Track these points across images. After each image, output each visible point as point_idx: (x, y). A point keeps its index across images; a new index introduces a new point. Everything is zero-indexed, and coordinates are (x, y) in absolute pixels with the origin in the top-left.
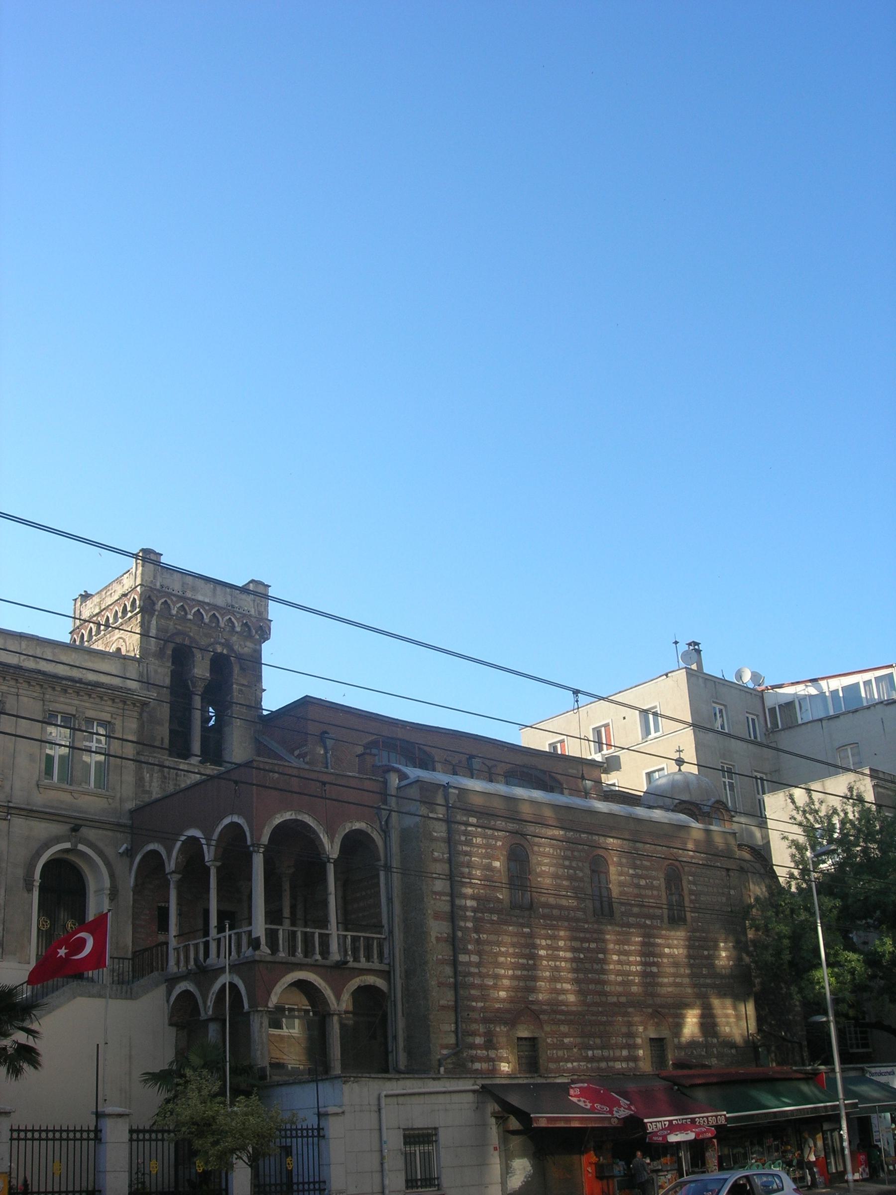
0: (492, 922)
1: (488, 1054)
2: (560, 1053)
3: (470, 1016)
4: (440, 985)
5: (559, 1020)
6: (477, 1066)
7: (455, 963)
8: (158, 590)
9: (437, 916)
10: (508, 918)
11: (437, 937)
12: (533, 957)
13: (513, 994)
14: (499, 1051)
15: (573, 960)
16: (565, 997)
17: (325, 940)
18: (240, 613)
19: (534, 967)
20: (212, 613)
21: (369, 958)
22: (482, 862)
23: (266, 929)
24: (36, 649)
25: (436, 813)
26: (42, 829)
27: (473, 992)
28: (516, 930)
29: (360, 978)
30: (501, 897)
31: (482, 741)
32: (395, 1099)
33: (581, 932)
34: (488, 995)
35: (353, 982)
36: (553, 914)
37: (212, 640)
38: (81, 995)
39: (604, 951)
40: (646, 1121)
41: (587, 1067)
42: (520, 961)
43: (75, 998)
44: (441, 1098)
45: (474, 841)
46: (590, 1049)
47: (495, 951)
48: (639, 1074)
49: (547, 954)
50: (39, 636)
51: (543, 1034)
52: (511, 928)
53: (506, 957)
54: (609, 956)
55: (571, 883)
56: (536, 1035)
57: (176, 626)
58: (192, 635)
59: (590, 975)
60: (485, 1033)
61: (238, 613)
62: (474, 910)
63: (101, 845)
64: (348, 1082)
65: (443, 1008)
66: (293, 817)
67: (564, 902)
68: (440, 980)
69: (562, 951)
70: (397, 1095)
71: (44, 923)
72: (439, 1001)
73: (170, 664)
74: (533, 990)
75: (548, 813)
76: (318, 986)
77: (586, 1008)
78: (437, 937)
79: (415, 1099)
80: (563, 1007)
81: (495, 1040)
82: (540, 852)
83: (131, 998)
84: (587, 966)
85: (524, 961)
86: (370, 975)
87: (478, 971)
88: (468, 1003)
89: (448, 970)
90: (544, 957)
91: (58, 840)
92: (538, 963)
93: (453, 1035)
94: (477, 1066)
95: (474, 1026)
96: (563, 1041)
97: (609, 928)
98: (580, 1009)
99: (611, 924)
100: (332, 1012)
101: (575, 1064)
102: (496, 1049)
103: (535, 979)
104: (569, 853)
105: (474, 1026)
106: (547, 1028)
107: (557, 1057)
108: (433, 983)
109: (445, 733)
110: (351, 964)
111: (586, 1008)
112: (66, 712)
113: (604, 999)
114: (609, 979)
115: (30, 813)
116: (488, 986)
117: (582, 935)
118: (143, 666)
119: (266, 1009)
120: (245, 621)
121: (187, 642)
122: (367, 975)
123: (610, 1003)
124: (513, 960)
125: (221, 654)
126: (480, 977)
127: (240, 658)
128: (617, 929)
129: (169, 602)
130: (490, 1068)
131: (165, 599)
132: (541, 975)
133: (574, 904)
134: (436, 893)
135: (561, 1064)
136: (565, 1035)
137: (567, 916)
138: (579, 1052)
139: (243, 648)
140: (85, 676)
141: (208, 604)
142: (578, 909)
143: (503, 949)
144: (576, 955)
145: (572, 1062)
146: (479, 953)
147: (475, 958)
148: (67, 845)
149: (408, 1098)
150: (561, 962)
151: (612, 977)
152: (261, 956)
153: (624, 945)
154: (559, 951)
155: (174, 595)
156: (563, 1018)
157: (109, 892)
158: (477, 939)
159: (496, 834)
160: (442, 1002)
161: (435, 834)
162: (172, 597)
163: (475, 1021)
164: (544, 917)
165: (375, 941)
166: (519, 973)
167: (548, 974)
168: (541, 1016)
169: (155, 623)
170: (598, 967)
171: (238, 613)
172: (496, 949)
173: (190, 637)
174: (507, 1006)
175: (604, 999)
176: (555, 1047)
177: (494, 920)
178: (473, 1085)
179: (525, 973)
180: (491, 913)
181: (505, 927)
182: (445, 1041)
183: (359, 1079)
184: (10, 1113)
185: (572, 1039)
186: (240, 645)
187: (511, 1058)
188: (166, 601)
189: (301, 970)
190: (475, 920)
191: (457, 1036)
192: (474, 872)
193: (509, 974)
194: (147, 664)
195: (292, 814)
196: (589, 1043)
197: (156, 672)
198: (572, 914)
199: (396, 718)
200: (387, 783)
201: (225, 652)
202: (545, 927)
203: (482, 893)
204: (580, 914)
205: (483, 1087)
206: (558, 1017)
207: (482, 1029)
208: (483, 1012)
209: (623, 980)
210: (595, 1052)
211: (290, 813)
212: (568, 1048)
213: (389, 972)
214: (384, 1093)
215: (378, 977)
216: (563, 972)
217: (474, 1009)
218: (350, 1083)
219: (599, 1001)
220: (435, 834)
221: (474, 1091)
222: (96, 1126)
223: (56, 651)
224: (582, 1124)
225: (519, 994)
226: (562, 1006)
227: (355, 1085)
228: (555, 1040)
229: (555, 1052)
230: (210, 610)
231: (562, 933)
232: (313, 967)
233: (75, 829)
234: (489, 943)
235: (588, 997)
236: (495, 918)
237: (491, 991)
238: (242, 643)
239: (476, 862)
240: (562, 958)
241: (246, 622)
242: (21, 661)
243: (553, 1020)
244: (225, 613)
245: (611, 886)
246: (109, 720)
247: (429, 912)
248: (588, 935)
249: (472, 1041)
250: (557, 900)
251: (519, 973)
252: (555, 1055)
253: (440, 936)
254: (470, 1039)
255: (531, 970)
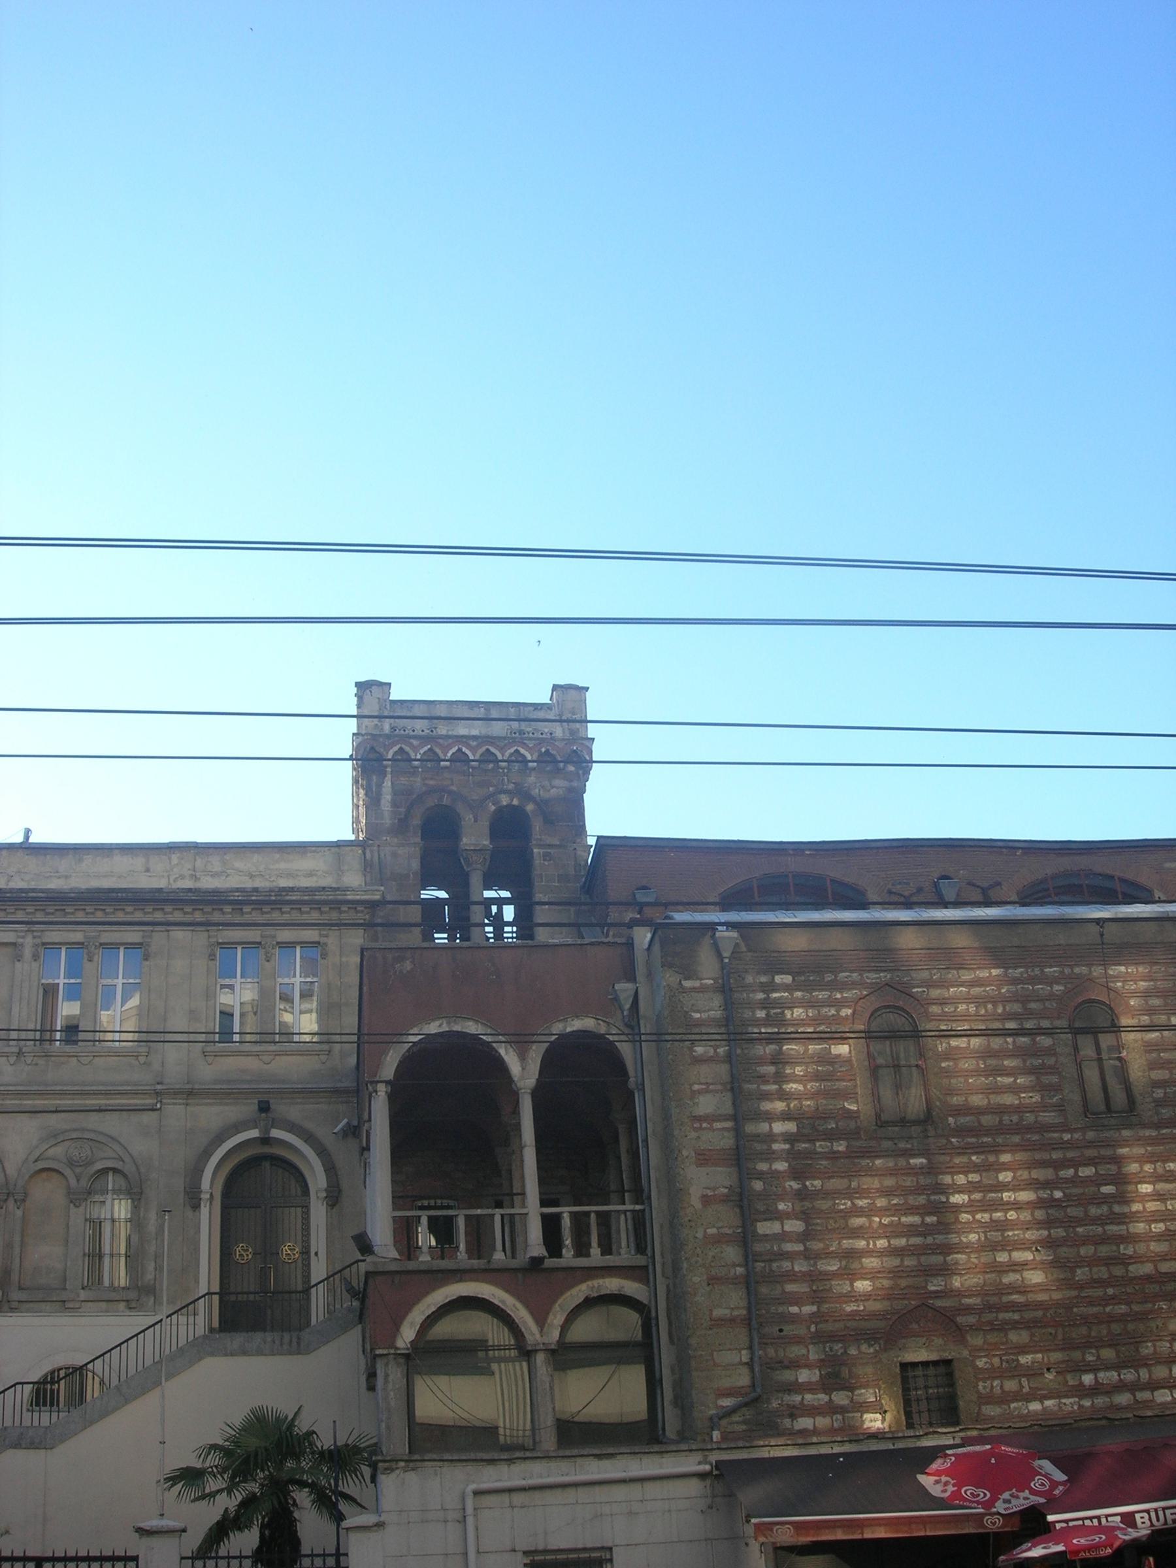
0: (834, 1156)
1: (830, 1399)
2: (1011, 1385)
3: (785, 1333)
4: (713, 1281)
5: (1006, 1322)
6: (805, 1423)
7: (745, 1238)
8: (387, 737)
9: (704, 1159)
10: (873, 1143)
11: (704, 1197)
12: (942, 1210)
13: (886, 1283)
14: (857, 1392)
15: (1039, 1204)
16: (1018, 1276)
17: (513, 1225)
18: (535, 739)
19: (944, 1227)
20: (484, 749)
21: (607, 1249)
22: (807, 1050)
23: (395, 1219)
24: (195, 860)
25: (698, 979)
26: (212, 1115)
27: (790, 1288)
28: (891, 1164)
29: (590, 1283)
30: (854, 1107)
31: (964, 846)
32: (505, 1498)
33: (1054, 1149)
34: (830, 1290)
35: (574, 1291)
36: (982, 1126)
37: (491, 789)
38: (212, 1354)
39: (1120, 1180)
40: (1050, 1518)
41: (1081, 1407)
42: (903, 1219)
43: (200, 1359)
44: (619, 1492)
45: (789, 1016)
46: (1086, 1372)
47: (842, 1207)
48: (1149, 1413)
49: (970, 1200)
50: (198, 841)
51: (966, 1353)
52: (878, 1162)
53: (868, 1216)
54: (1131, 1188)
55: (1024, 1061)
56: (947, 1355)
57: (427, 782)
58: (454, 788)
59: (1080, 1230)
60: (822, 1360)
61: (530, 739)
62: (789, 1138)
63: (310, 1125)
64: (392, 1470)
65: (719, 1322)
66: (445, 1028)
67: (1009, 1099)
68: (713, 1273)
69: (1008, 1191)
70: (510, 1490)
71: (242, 1252)
72: (711, 1310)
73: (418, 840)
74: (946, 1271)
75: (960, 940)
76: (500, 1304)
77: (1074, 1293)
78: (704, 1197)
79: (550, 1497)
80: (1014, 1297)
81: (845, 1372)
82: (944, 1014)
83: (299, 1349)
84: (1072, 1212)
85: (916, 1219)
86: (611, 1276)
87: (802, 1248)
88: (780, 1309)
89: (732, 1253)
90: (963, 1205)
91: (237, 1128)
92: (950, 1218)
93: (745, 1371)
94: (805, 1423)
95: (796, 1351)
96: (1018, 1360)
97: (1126, 1133)
98: (1057, 1296)
99: (1129, 1126)
100: (529, 1348)
101: (1048, 1403)
102: (851, 1389)
103: (947, 1249)
104: (1016, 1007)
105: (796, 1351)
106: (977, 1341)
107: (1003, 1391)
108: (696, 1279)
109: (886, 848)
110: (550, 1263)
111: (1074, 1293)
112: (245, 940)
113: (1118, 1271)
114: (1131, 1230)
115: (190, 1094)
116: (826, 1273)
117: (1055, 1155)
118: (372, 852)
119: (392, 1351)
120: (543, 750)
121: (446, 801)
122: (603, 1277)
123: (1135, 1278)
124: (885, 1221)
125: (510, 806)
126: (807, 1258)
127: (543, 805)
128: (1147, 1134)
129: (407, 749)
130: (835, 1425)
131: (398, 747)
132: (956, 1240)
133: (1034, 1100)
134: (699, 1119)
135: (1012, 1405)
136: (1023, 1350)
137: (1017, 1124)
138: (1060, 1378)
139: (549, 791)
140: (274, 883)
141: (475, 738)
142: (1044, 1107)
143: (861, 1203)
144: (1044, 1194)
145: (1042, 1399)
146: (805, 1216)
147: (794, 1226)
148: (254, 1133)
149: (537, 1495)
150: (1006, 1211)
151: (1140, 1227)
152: (374, 1263)
153: (1165, 1161)
154: (1002, 1191)
155: (415, 737)
156: (1016, 1317)
157: (325, 1195)
158: (799, 1190)
159: (838, 996)
160: (718, 1313)
161: (697, 1015)
162: (412, 741)
163: (798, 1340)
164: (960, 1131)
165: (622, 1217)
166: (902, 1242)
167: (973, 1237)
168: (959, 1319)
169: (390, 784)
170: (1099, 1211)
171: (530, 739)
172: (845, 1204)
173: (450, 792)
174: (875, 1306)
175: (1118, 1271)
176: (993, 1373)
177: (838, 1152)
178: (700, 1463)
179: (917, 1240)
180: (831, 1140)
181: (864, 1162)
182: (726, 1383)
183: (419, 1464)
184: (638, 1513)
185: (1040, 1356)
186: (543, 787)
187: (887, 1402)
188: (401, 749)
189: (461, 1280)
190: (791, 1155)
191: (752, 1370)
192: (788, 1071)
193: (878, 1245)
194: (379, 846)
195: (440, 1026)
196: (1084, 1360)
197: (394, 855)
198: (1030, 1118)
199: (736, 839)
200: (632, 944)
201: (515, 802)
202: (964, 1150)
203: (809, 1105)
204: (1049, 1117)
205: (719, 1465)
206: (1001, 1316)
207: (814, 1354)
208: (816, 1324)
209: (1167, 1229)
210: (1101, 1375)
211: (437, 1023)
212: (1032, 1373)
213: (646, 1268)
214: (473, 1487)
215: (626, 1278)
216: (1012, 1230)
217: (794, 1319)
218: (397, 1472)
219: (1106, 1276)
220: (697, 1015)
221: (702, 1476)
222: (338, 1549)
223: (227, 857)
224: (897, 1532)
225: (903, 1283)
226: (1011, 1294)
227: (412, 1477)
228: (996, 1361)
229: (996, 1383)
230: (479, 746)
231: (1006, 1158)
232: (489, 1274)
233: (264, 1107)
234: (825, 1194)
235: (1079, 1271)
236: (841, 1146)
237: (833, 1283)
238: (546, 783)
239: (793, 1052)
240: (1008, 1203)
241: (547, 751)
242: (172, 881)
243: (990, 1323)
244: (505, 745)
245: (1124, 1054)
246: (317, 939)
247: (685, 1153)
248: (1070, 1154)
249: (793, 1378)
250: (991, 1096)
251: (902, 1242)
252: (997, 1390)
253: (710, 1193)
254: (787, 1376)
255: (930, 1234)
